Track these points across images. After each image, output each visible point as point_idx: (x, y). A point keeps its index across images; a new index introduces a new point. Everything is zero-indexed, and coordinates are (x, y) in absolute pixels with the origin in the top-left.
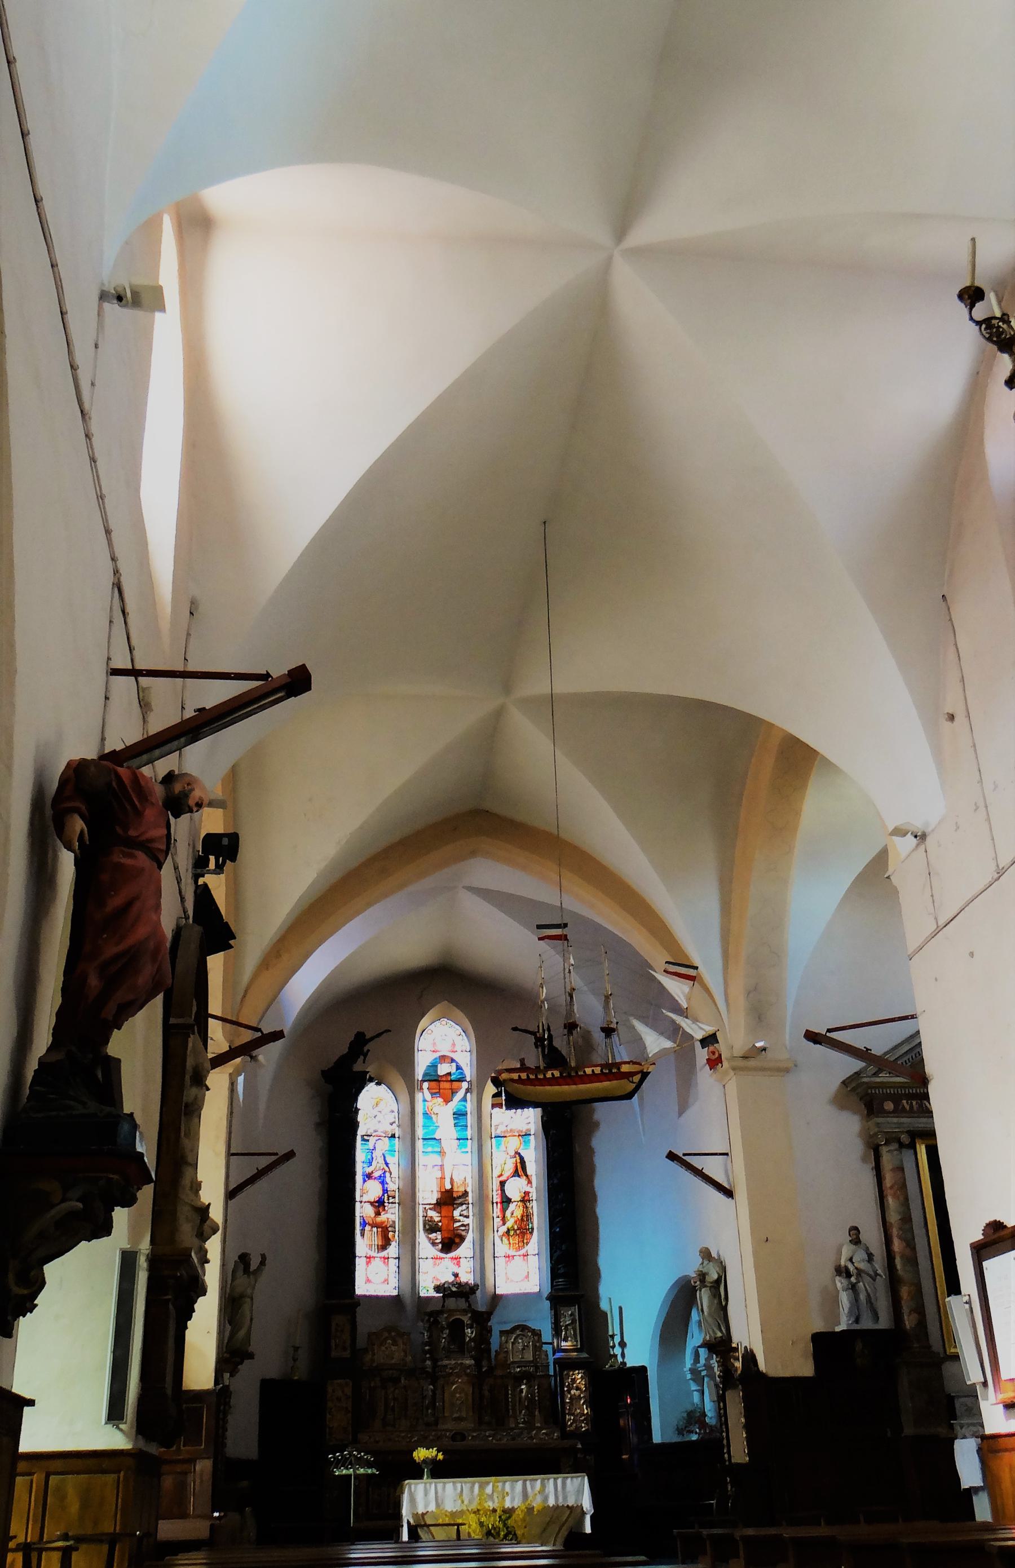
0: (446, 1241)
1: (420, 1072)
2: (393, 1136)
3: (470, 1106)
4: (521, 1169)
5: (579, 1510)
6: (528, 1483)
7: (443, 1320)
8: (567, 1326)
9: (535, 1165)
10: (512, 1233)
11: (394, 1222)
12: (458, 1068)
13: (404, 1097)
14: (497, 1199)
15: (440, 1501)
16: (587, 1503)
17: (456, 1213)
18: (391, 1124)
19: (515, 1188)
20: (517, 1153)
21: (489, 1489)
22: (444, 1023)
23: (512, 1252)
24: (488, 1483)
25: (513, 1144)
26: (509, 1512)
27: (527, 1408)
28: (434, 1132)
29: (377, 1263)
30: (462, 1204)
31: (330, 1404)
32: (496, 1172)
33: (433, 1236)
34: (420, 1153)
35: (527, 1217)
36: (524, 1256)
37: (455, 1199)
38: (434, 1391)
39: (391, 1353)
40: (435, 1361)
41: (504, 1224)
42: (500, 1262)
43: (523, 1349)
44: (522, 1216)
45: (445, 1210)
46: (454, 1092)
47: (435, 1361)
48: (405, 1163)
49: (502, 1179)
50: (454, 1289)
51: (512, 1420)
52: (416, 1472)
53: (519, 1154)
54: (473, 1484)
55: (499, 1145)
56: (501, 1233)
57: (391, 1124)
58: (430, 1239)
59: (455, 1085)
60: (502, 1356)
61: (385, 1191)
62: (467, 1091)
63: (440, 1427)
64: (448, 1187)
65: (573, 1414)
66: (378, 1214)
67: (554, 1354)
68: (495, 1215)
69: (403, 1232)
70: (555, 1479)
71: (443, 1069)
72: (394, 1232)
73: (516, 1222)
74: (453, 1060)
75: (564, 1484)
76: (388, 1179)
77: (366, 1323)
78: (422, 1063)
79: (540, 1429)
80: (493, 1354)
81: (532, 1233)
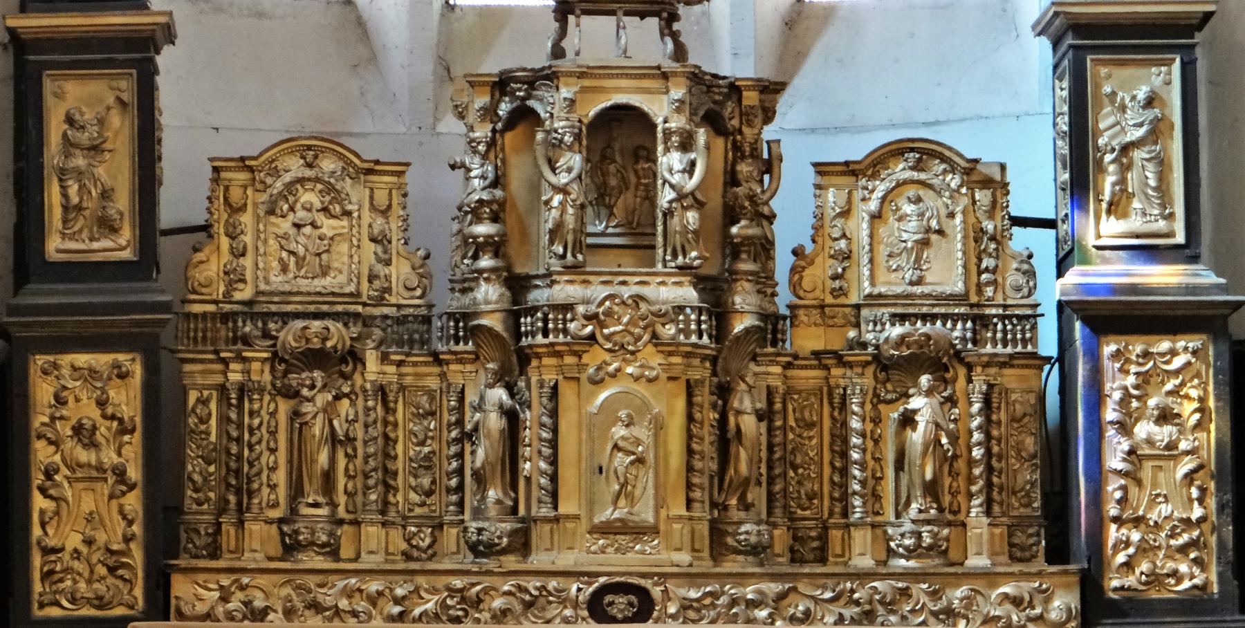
7: (558, 109)
8: (1126, 149)
27: (932, 489)
31: (42, 453)
38: (512, 418)
43: (925, 243)
51: (861, 538)
60: (819, 274)
63: (539, 559)
65: (1138, 521)
67: (1062, 267)
79: (989, 577)
80: (783, 262)
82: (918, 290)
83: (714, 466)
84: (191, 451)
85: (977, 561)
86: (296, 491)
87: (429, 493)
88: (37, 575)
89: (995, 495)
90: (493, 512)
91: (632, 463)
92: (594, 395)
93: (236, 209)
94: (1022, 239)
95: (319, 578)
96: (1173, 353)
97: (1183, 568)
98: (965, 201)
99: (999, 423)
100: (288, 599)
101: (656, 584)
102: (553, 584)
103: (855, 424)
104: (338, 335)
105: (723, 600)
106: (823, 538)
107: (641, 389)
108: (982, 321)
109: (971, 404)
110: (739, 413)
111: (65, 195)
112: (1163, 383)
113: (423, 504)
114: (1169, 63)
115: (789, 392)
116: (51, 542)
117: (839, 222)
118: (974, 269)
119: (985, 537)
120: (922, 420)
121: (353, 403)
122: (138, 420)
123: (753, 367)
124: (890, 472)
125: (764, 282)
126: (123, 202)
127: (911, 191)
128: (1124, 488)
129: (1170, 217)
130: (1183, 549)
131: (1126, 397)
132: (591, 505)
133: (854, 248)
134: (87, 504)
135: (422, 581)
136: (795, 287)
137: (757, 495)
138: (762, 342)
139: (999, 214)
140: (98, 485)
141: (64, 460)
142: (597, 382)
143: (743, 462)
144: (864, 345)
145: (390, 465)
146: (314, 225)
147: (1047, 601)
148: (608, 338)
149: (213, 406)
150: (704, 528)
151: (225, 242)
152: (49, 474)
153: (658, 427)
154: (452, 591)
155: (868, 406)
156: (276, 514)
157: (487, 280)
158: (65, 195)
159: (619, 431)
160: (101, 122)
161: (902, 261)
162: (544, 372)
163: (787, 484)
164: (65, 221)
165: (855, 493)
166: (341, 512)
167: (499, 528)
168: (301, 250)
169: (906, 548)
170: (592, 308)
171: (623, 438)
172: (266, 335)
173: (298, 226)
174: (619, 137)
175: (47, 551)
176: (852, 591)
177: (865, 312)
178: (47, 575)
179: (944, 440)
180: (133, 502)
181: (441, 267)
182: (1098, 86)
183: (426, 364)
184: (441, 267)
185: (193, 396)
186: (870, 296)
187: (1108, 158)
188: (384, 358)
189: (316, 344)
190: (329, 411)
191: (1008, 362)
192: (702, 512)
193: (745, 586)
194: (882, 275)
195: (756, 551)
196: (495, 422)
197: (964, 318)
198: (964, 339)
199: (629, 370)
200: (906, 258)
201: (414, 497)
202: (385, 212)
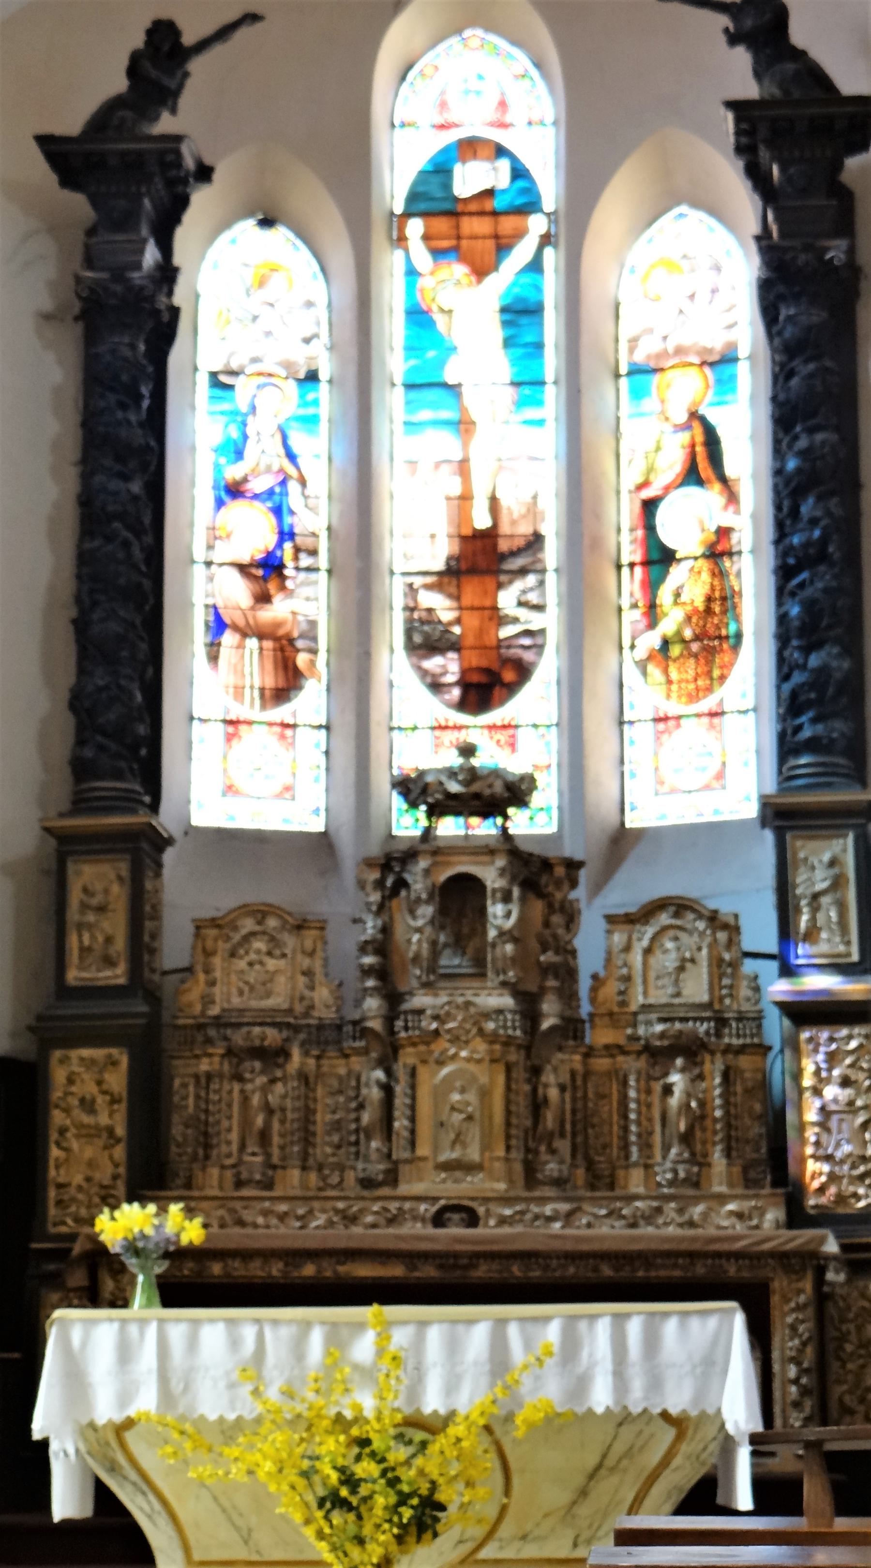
0: (475, 678)
1: (395, 182)
2: (312, 377)
3: (551, 288)
4: (705, 461)
5: (711, 1431)
6: (513, 1331)
7: (418, 880)
8: (816, 896)
9: (747, 451)
10: (675, 650)
11: (313, 624)
12: (519, 173)
13: (342, 256)
14: (631, 552)
15: (176, 1386)
16: (737, 1407)
17: (507, 600)
18: (307, 341)
19: (686, 520)
20: (694, 415)
21: (364, 1348)
22: (474, 43)
23: (673, 707)
24: (360, 1326)
25: (684, 388)
26: (419, 1429)
27: (686, 1139)
28: (441, 364)
29: (258, 740)
30: (523, 572)
31: (58, 1117)
32: (631, 477)
33: (434, 663)
34: (398, 427)
35: (722, 601)
36: (713, 715)
37: (503, 557)
38: (388, 1090)
39: (259, 983)
40: (393, 999)
41: (652, 625)
42: (640, 735)
43: (681, 969)
44: (709, 599)
45: (471, 592)
46: (503, 245)
47: (393, 999)
48: (345, 453)
49: (647, 494)
50: (454, 787)
52: (99, 1280)
53: (703, 420)
54: (307, 1325)
55: (638, 394)
56: (641, 653)
57: (307, 341)
58: (424, 673)
59: (507, 224)
60: (611, 989)
61: (285, 535)
62: (546, 240)
63: (404, 1189)
64: (482, 521)
65: (829, 1158)
66: (263, 598)
68: (625, 603)
69: (336, 651)
70: (620, 1320)
71: (469, 179)
72: (314, 652)
73: (689, 618)
74: (500, 151)
75: (652, 1342)
76: (294, 497)
77: (184, 894)
78: (400, 164)
79: (722, 1199)
80: (584, 985)
81: (736, 647)
82: (677, 1001)
83: (528, 1123)
84: (176, 1119)
85: (720, 1188)
86: (242, 1147)
87: (338, 1147)
88: (51, 1203)
89: (733, 1144)
90: (374, 1156)
91: (465, 1120)
92: (435, 1074)
93: (208, 954)
94: (749, 966)
95: (244, 1203)
96: (850, 1037)
97: (861, 1191)
98: (708, 939)
99: (735, 1094)
100: (222, 1218)
101: (481, 1205)
102: (407, 1205)
103: (632, 1094)
104: (273, 1036)
105: (528, 1216)
106: (612, 1176)
107: (472, 1067)
108: (721, 1022)
109: (713, 1079)
110: (546, 1086)
111: (81, 941)
112: (844, 1059)
113: (334, 1155)
114: (845, 836)
115: (587, 1075)
116: (61, 1180)
117: (623, 956)
118: (717, 987)
119: (724, 1173)
120: (678, 1091)
121: (285, 1084)
122: (125, 1094)
123: (560, 1056)
124: (658, 1128)
125: (569, 996)
126: (120, 944)
127: (671, 933)
128: (817, 1134)
129: (848, 943)
130: (862, 1178)
131: (817, 1072)
132: (436, 1149)
133: (633, 973)
134: (89, 1153)
135: (316, 1205)
136: (593, 1000)
137: (563, 1146)
138: (566, 1038)
139: (734, 949)
140: (96, 1140)
141: (73, 1123)
142: (441, 1063)
143: (550, 1119)
144: (638, 1039)
145: (311, 1128)
146: (261, 963)
147: (762, 1215)
148: (449, 1031)
149: (191, 1089)
150: (518, 1167)
151: (202, 977)
152: (63, 1131)
153: (485, 1094)
154: (337, 1211)
155: (642, 1083)
156: (229, 1162)
157: (371, 996)
158: (81, 941)
159: (456, 1097)
160: (106, 891)
161: (665, 981)
162: (408, 1057)
163: (586, 1137)
164: (81, 958)
165: (633, 1143)
166: (275, 1160)
167: (378, 1168)
168: (252, 981)
169: (668, 1180)
170: (436, 1012)
171: (458, 1102)
172: (226, 1038)
173: (251, 964)
174: (461, 897)
175: (60, 1186)
176: (621, 1209)
177: (641, 1017)
178: (59, 1203)
179: (694, 1104)
180: (119, 1152)
181: (349, 993)
182: (795, 854)
183: (337, 1058)
184: (349, 993)
185: (177, 1082)
186: (643, 1006)
187: (803, 902)
188: (306, 1054)
189: (257, 1043)
190: (265, 1090)
191: (741, 1050)
192: (517, 1155)
193: (545, 1205)
194: (652, 991)
195: (559, 1182)
196: (375, 1094)
197: (708, 1019)
198: (707, 1033)
199: (464, 1054)
200: (668, 978)
201: (328, 1150)
202: (311, 954)
